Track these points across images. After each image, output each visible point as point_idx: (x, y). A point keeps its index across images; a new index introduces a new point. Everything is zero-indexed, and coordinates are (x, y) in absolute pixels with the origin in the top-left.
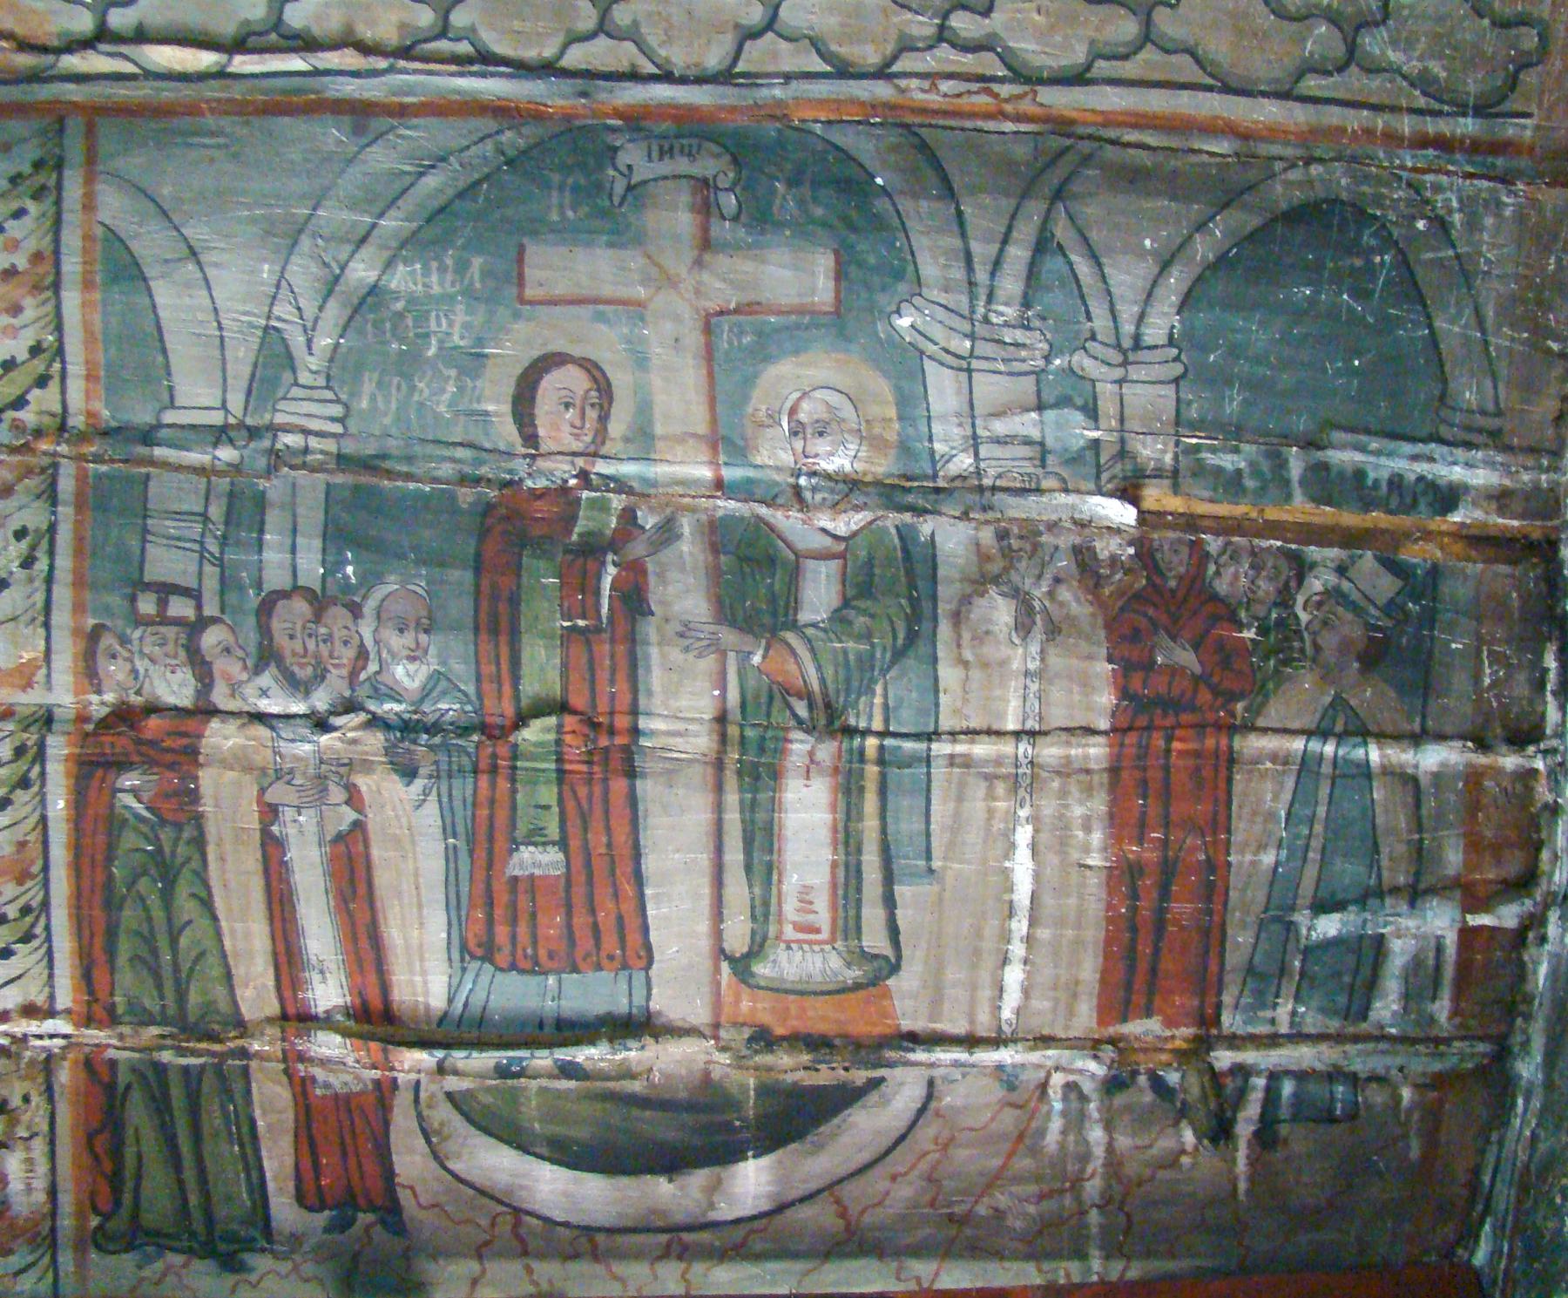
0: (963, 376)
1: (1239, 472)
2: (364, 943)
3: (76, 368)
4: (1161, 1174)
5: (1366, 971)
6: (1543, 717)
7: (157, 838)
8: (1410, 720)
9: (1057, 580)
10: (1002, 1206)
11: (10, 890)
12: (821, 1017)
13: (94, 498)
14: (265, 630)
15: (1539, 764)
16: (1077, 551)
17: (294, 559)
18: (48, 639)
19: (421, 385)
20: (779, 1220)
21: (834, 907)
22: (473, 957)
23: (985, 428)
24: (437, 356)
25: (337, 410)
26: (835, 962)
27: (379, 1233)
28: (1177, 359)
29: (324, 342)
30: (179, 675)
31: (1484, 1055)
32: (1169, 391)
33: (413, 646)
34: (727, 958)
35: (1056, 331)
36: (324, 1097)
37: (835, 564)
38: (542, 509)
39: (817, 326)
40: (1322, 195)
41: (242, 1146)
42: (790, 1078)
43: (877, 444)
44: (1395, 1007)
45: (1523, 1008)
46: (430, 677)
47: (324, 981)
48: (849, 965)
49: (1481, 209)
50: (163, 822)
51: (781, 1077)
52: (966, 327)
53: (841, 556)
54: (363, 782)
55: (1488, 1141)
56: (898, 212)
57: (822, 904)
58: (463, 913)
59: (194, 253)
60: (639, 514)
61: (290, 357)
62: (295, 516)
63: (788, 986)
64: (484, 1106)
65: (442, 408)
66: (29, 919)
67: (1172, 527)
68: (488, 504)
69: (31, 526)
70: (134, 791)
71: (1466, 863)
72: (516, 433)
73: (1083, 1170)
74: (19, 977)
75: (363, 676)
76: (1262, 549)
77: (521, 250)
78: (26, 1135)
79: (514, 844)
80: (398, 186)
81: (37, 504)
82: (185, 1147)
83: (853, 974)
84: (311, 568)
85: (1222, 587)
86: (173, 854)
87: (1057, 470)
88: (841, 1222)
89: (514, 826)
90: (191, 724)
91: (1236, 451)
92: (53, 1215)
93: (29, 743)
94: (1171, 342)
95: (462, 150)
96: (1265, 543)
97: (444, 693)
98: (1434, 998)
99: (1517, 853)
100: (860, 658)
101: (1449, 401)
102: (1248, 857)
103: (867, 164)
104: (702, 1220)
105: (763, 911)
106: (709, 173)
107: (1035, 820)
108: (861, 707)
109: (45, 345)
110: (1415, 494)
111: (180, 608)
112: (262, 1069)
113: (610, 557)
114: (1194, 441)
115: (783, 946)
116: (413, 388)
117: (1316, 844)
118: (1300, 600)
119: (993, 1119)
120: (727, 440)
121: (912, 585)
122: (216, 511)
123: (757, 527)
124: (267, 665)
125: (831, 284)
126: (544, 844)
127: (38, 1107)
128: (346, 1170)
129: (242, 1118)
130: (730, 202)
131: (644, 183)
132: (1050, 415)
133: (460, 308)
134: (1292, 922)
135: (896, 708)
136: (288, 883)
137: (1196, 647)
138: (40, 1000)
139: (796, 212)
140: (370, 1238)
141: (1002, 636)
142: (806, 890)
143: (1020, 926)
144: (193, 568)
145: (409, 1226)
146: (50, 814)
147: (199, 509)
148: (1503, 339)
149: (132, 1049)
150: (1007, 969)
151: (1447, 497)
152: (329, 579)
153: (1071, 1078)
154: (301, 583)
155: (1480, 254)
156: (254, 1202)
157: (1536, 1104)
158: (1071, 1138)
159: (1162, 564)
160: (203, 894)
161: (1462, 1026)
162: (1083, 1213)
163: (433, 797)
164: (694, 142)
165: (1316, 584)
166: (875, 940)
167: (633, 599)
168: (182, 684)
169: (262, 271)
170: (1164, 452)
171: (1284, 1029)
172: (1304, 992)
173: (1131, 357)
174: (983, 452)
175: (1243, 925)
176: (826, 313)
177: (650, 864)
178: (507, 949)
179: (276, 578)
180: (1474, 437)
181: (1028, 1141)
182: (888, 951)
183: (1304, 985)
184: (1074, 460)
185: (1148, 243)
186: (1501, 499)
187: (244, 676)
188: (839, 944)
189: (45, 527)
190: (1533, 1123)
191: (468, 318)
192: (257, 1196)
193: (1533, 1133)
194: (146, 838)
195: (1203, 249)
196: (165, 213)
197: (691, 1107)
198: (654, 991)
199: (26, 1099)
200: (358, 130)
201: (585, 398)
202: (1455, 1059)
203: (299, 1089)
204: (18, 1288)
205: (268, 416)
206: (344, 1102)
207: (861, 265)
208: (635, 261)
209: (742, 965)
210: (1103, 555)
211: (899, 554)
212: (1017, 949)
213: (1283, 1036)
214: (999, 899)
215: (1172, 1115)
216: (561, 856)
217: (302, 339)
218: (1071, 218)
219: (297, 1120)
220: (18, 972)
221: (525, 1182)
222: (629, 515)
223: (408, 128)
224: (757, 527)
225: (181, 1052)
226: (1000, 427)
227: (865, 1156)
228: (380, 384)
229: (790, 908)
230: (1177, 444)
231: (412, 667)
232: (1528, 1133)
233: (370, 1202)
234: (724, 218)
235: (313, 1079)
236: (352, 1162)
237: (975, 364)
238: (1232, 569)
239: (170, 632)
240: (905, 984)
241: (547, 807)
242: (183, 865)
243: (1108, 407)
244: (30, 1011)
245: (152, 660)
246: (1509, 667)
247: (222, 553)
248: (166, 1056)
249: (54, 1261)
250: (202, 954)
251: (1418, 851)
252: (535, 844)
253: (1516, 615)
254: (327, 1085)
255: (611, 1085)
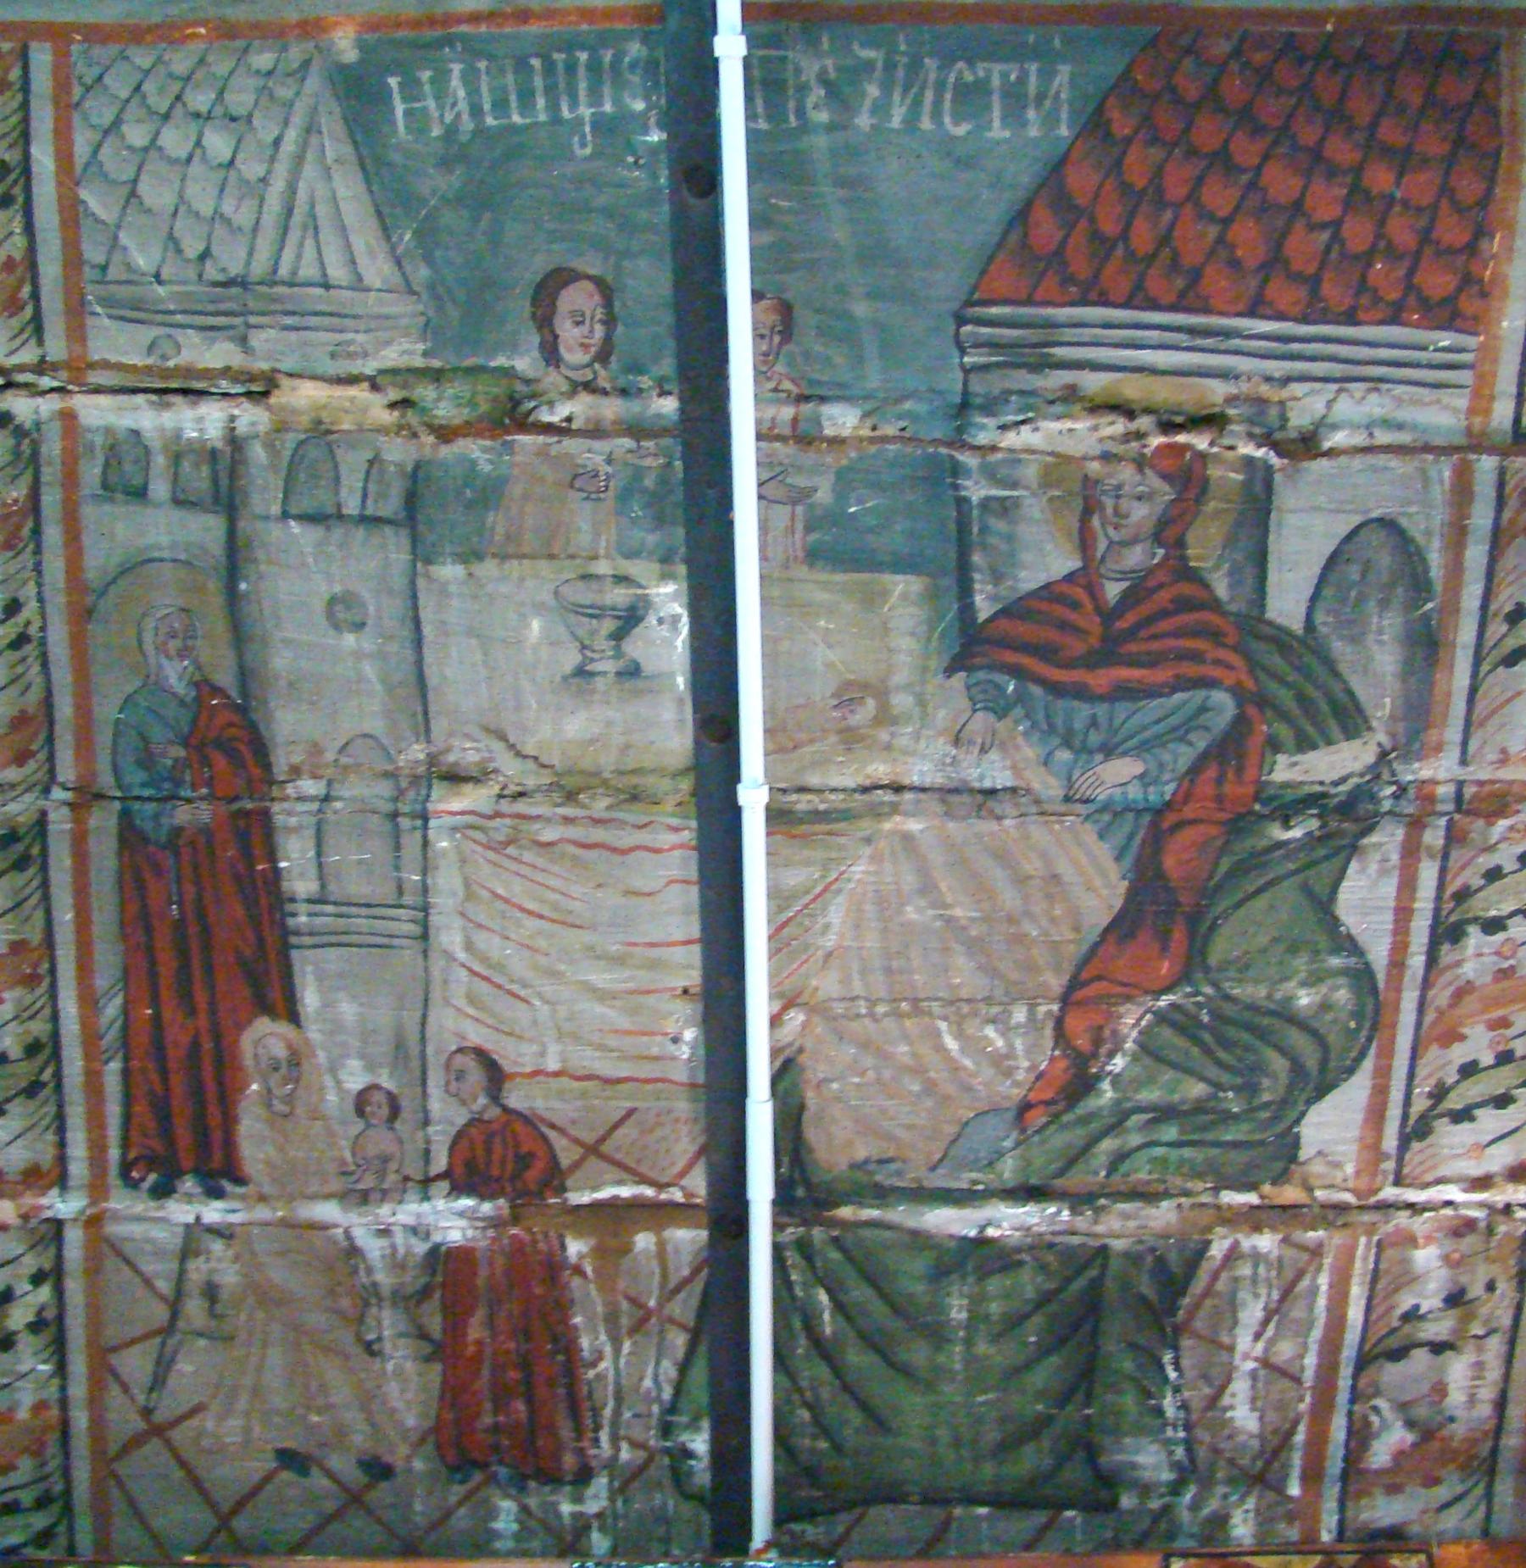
78: (1480, 1332)
92: (1498, 1431)
127: (1503, 1295)
199: (1491, 1287)
204: (1440, 1527)
220: (1514, 1125)
249: (1489, 1495)
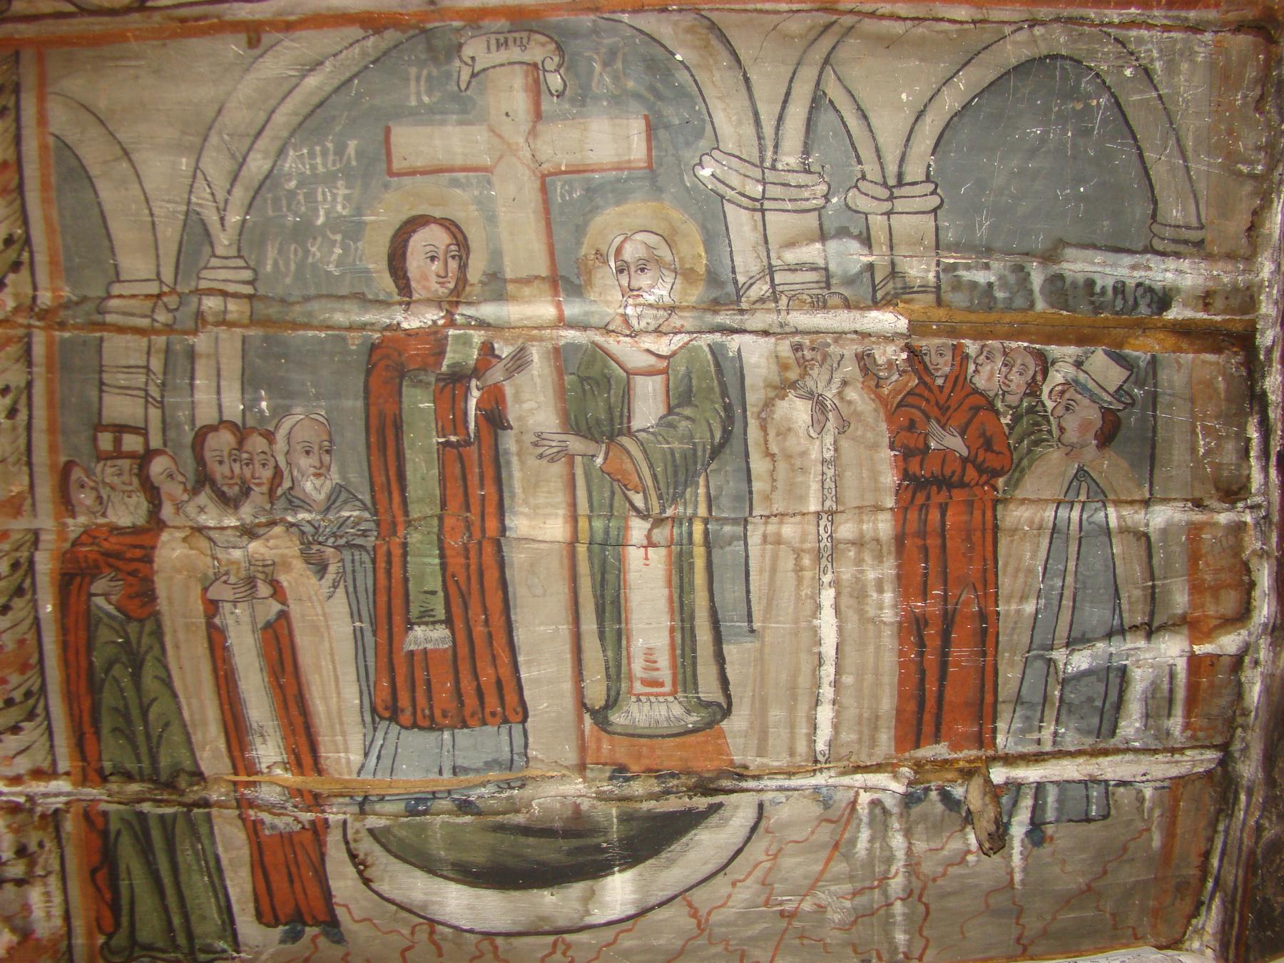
0: (758, 215)
1: (990, 285)
2: (294, 711)
3: (41, 258)
4: (951, 870)
5: (1113, 697)
6: (1248, 477)
7: (125, 631)
8: (1140, 486)
9: (845, 383)
10: (823, 903)
11: (15, 679)
12: (669, 755)
13: (61, 361)
14: (200, 460)
15: (1248, 518)
16: (860, 357)
17: (219, 399)
18: (31, 475)
19: (313, 249)
20: (643, 921)
21: (674, 666)
22: (382, 718)
23: (779, 258)
24: (324, 225)
25: (247, 275)
26: (677, 710)
27: (323, 942)
28: (934, 193)
29: (234, 218)
30: (134, 499)
31: (1210, 761)
32: (929, 221)
33: (318, 465)
34: (588, 710)
35: (831, 175)
36: (271, 836)
37: (659, 379)
38: (415, 348)
39: (634, 179)
40: (1045, 52)
41: (210, 876)
42: (646, 806)
43: (687, 275)
44: (1137, 725)
45: (1240, 720)
46: (333, 490)
47: (265, 742)
48: (688, 712)
49: (1177, 56)
50: (129, 618)
51: (637, 805)
52: (757, 173)
53: (665, 372)
54: (284, 579)
55: (1215, 831)
56: (695, 81)
57: (664, 661)
58: (372, 678)
59: (126, 153)
60: (496, 346)
61: (207, 233)
62: (218, 363)
63: (639, 731)
64: (400, 839)
65: (331, 268)
66: (31, 702)
67: (936, 334)
68: (373, 344)
69: (13, 385)
70: (106, 595)
71: (1191, 602)
72: (392, 285)
73: (888, 871)
74: (28, 748)
75: (279, 492)
76: (1012, 350)
77: (388, 131)
78: (42, 873)
79: (409, 625)
80: (286, 87)
81: (17, 366)
82: (167, 880)
83: (692, 720)
84: (233, 406)
85: (980, 382)
86: (139, 642)
87: (842, 290)
88: (694, 921)
89: (408, 611)
90: (145, 540)
91: (987, 267)
93: (22, 560)
94: (928, 179)
95: (335, 55)
96: (1014, 345)
97: (345, 502)
98: (1169, 715)
99: (1233, 593)
100: (684, 457)
101: (1159, 218)
102: (1013, 607)
103: (667, 43)
104: (581, 924)
105: (616, 672)
106: (538, 59)
107: (836, 583)
108: (688, 496)
109: (15, 237)
110: (1135, 298)
111: (132, 443)
112: (220, 816)
113: (474, 383)
114: (952, 261)
115: (634, 699)
116: (307, 252)
117: (1068, 593)
118: (1046, 390)
119: (813, 833)
120: (566, 280)
121: (724, 393)
122: (156, 364)
123: (594, 355)
124: (203, 486)
125: (644, 145)
126: (434, 623)
127: (50, 851)
128: (294, 892)
129: (209, 852)
130: (555, 81)
131: (484, 70)
132: (833, 245)
133: (340, 183)
134: (1050, 659)
135: (717, 498)
136: (231, 664)
137: (962, 434)
138: (46, 765)
139: (612, 87)
140: (316, 948)
141: (802, 432)
142: (649, 652)
143: (828, 671)
144: (140, 412)
145: (347, 937)
146: (42, 615)
147: (142, 363)
148: (1200, 166)
149: (120, 803)
150: (819, 708)
151: (1163, 300)
152: (248, 414)
153: (876, 796)
154: (225, 418)
155: (1178, 94)
156: (223, 922)
157: (1258, 798)
158: (877, 845)
159: (931, 367)
160: (164, 675)
161: (1193, 737)
162: (890, 905)
163: (341, 590)
164: (525, 35)
165: (1057, 377)
166: (709, 689)
167: (495, 419)
168: (137, 506)
169: (181, 163)
170: (928, 271)
171: (1048, 747)
172: (1063, 718)
173: (896, 192)
174: (778, 278)
175: (1012, 664)
176: (641, 168)
177: (520, 636)
178: (408, 712)
179: (206, 416)
180: (1181, 248)
181: (843, 850)
182: (721, 699)
183: (1064, 711)
184: (850, 281)
185: (904, 96)
186: (1206, 299)
187: (185, 497)
188: (680, 695)
189: (23, 384)
190: (1257, 814)
191: (347, 192)
192: (225, 916)
193: (1257, 822)
194: (117, 632)
195: (950, 102)
196: (102, 122)
197: (567, 834)
198: (531, 740)
199: (41, 845)
200: (253, 43)
201: (447, 251)
202: (1188, 765)
203: (251, 830)
205: (193, 284)
206: (287, 839)
207: (667, 127)
208: (480, 135)
209: (601, 717)
210: (881, 360)
211: (712, 368)
212: (827, 692)
213: (1047, 753)
214: (809, 651)
215: (959, 822)
216: (447, 632)
217: (215, 218)
218: (839, 79)
219: (251, 855)
221: (435, 899)
222: (488, 350)
223: (292, 40)
224: (594, 355)
225: (158, 802)
226: (791, 256)
227: (710, 868)
228: (280, 252)
229: (638, 667)
230: (938, 264)
231: (318, 482)
232: (1252, 823)
233: (314, 917)
234: (552, 94)
235: (262, 822)
236: (297, 885)
237: (767, 205)
238: (988, 367)
239: (125, 463)
240: (736, 724)
241: (433, 593)
242: (146, 653)
243: (879, 234)
244: (38, 774)
245: (113, 488)
246: (1219, 438)
247: (162, 396)
248: (146, 807)
250: (167, 725)
251: (1152, 597)
252: (426, 624)
253: (1223, 396)
254: (273, 827)
255: (499, 818)
